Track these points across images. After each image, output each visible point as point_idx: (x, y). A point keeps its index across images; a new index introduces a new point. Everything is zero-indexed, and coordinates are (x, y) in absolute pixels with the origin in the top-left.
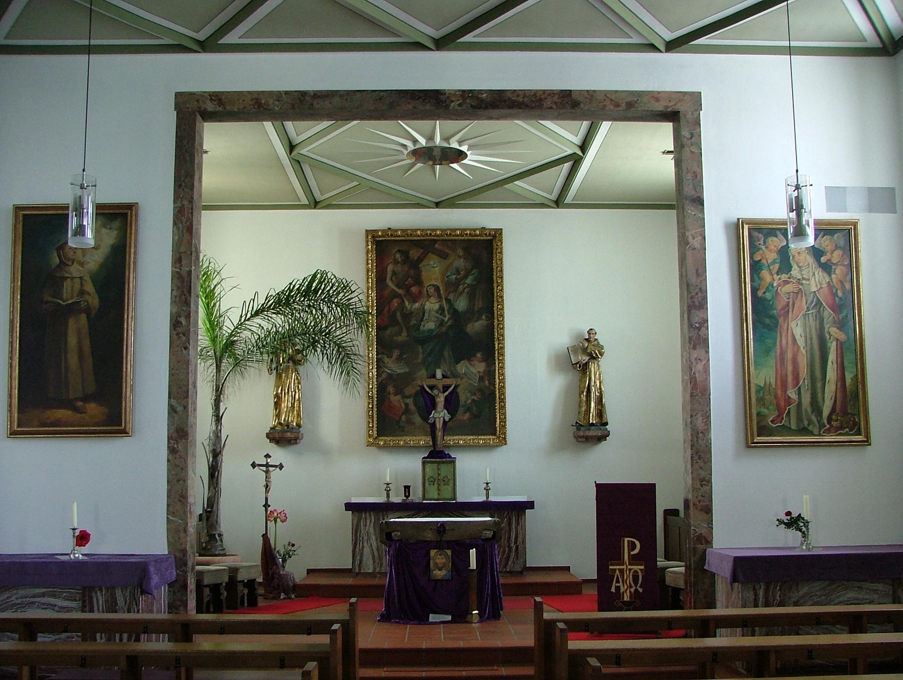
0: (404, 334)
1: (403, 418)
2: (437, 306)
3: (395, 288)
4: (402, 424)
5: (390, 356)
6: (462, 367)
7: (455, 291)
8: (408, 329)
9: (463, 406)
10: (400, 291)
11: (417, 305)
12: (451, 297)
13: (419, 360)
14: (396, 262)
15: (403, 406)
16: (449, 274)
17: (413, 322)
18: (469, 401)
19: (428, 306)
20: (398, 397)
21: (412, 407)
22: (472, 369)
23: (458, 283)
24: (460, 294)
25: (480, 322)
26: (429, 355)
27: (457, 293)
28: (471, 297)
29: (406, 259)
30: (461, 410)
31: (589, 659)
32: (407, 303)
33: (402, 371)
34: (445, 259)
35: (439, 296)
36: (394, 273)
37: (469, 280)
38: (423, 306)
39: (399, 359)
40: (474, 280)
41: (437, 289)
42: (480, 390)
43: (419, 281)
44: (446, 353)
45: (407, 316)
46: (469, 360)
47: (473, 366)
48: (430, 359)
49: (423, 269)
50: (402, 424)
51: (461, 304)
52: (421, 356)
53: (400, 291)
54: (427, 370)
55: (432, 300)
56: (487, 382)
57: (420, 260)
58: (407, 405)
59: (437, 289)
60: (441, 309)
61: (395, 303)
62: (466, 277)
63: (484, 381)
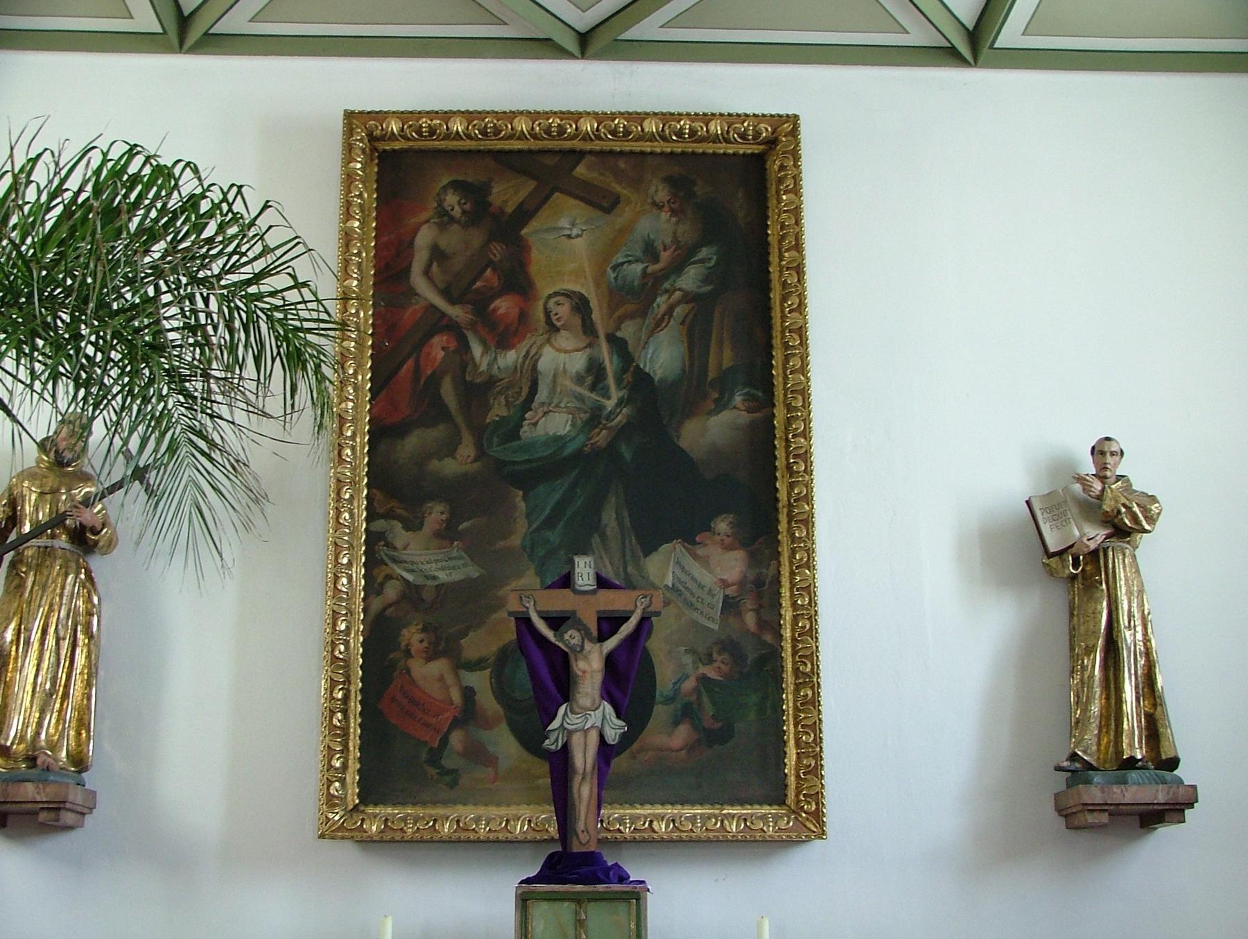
0: (467, 450)
1: (456, 739)
2: (578, 362)
4: (448, 762)
5: (413, 525)
7: (643, 313)
8: (480, 433)
9: (669, 700)
10: (456, 312)
11: (510, 358)
12: (628, 331)
13: (516, 540)
14: (444, 219)
15: (456, 696)
17: (498, 410)
18: (689, 684)
19: (549, 359)
20: (439, 666)
21: (488, 701)
22: (696, 570)
24: (658, 325)
25: (726, 416)
26: (550, 523)
27: (649, 321)
31: (435, 464)
32: (477, 350)
33: (457, 576)
34: (608, 211)
35: (588, 328)
36: (437, 254)
37: (690, 279)
39: (447, 534)
40: (706, 280)
41: (581, 305)
42: (730, 646)
43: (517, 280)
44: (609, 517)
45: (477, 392)
46: (689, 538)
47: (704, 561)
48: (554, 536)
50: (448, 762)
52: (521, 527)
53: (456, 312)
55: (565, 340)
56: (750, 620)
57: (524, 214)
59: (581, 305)
60: (595, 371)
61: (438, 348)
62: (678, 267)
63: (739, 614)
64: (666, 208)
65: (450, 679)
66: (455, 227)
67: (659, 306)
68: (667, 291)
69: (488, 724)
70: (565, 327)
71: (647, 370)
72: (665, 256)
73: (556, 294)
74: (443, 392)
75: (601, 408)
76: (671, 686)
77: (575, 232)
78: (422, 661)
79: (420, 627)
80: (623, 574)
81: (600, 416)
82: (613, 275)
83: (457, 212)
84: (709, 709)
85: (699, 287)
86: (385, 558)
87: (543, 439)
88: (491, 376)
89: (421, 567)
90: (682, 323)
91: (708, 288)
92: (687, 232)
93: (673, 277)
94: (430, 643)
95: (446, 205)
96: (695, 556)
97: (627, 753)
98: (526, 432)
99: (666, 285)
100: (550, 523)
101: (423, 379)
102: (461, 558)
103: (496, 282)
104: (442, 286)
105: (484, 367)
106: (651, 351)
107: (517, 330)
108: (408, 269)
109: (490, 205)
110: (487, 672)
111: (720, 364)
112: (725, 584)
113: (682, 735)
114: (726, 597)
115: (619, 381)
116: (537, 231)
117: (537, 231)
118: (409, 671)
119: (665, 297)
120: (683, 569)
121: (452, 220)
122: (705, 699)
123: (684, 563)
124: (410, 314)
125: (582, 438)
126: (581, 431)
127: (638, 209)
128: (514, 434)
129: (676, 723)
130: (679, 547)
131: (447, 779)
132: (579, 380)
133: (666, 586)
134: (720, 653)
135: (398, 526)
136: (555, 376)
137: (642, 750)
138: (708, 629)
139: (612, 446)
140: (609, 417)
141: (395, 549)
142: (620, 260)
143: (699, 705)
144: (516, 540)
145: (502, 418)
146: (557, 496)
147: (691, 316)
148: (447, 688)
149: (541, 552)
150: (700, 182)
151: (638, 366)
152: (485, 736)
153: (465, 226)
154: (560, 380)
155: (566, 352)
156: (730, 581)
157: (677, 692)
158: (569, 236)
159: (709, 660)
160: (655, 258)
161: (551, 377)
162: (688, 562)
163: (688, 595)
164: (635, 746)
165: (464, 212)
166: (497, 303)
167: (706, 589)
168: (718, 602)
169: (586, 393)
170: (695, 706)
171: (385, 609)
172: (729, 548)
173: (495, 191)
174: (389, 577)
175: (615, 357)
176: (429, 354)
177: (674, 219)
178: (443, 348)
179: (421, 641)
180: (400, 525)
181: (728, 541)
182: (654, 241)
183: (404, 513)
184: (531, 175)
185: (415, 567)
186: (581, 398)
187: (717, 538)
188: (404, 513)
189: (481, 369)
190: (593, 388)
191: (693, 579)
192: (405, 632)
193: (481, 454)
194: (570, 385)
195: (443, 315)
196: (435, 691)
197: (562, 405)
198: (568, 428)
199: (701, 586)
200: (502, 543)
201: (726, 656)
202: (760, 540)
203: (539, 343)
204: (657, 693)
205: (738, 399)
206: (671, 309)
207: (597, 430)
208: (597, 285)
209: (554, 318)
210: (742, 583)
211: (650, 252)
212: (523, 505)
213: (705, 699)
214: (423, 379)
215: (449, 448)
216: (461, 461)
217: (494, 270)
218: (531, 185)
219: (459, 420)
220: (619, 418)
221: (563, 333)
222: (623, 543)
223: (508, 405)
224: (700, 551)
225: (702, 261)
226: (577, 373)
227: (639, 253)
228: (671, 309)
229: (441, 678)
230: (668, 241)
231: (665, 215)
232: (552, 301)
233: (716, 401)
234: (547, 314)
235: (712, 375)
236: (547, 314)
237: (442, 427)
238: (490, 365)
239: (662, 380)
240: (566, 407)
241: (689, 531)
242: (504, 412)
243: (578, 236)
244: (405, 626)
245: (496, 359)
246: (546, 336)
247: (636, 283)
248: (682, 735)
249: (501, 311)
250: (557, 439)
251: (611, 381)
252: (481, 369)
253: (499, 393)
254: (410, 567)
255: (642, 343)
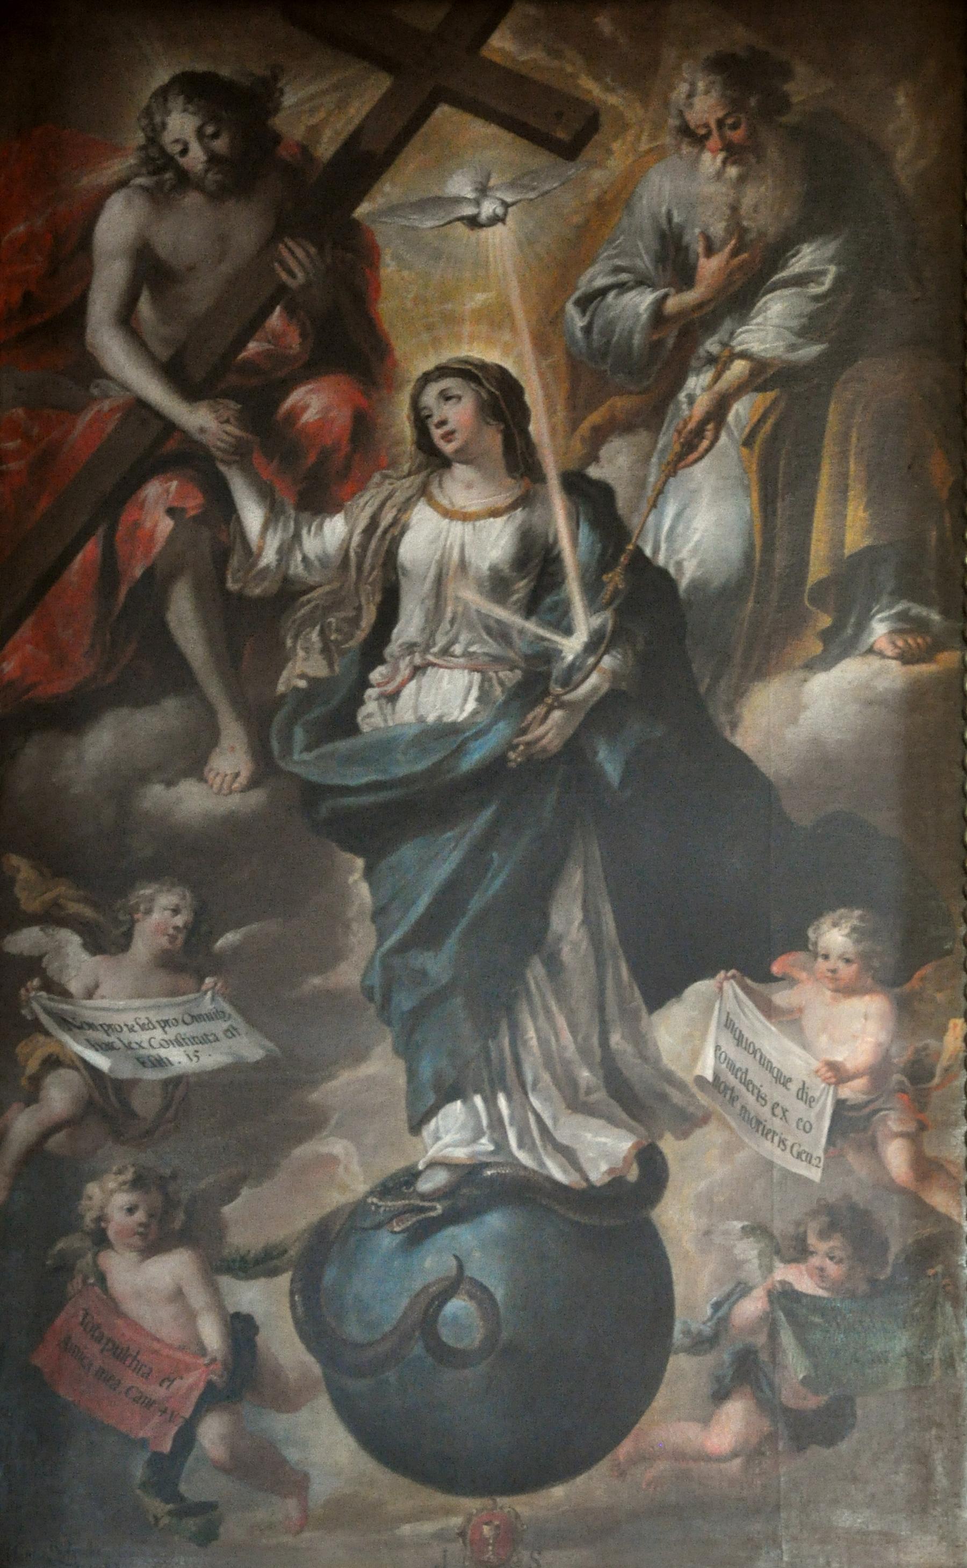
0: (231, 760)
1: (212, 1432)
2: (494, 543)
3: (155, 391)
4: (195, 1486)
5: (107, 939)
6: (693, 1034)
7: (654, 414)
8: (260, 722)
9: (701, 1344)
10: (200, 420)
11: (334, 532)
12: (615, 465)
13: (349, 974)
14: (164, 175)
15: (211, 1334)
16: (596, 277)
17: (304, 665)
18: (751, 1307)
19: (424, 537)
20: (174, 1268)
21: (284, 1345)
22: (772, 1041)
23: (676, 345)
24: (690, 447)
25: (850, 671)
26: (428, 933)
27: (667, 438)
28: (781, 479)
29: (252, 156)
30: (684, 1372)
31: (155, 795)
32: (252, 516)
33: (212, 1059)
34: (570, 151)
35: (520, 460)
36: (151, 271)
37: (768, 329)
38: (382, 544)
39: (187, 960)
40: (808, 330)
41: (502, 399)
42: (849, 1223)
43: (349, 340)
44: (567, 919)
45: (255, 618)
46: (757, 971)
47: (790, 1021)
48: (437, 964)
49: (389, 239)
50: (195, 1486)
51: (699, 526)
52: (362, 941)
53: (200, 420)
54: (407, 1050)
55: (464, 488)
56: (897, 1157)
57: (363, 164)
58: (241, 1329)
59: (502, 399)
60: (534, 574)
61: (158, 510)
62: (739, 298)
63: (872, 1148)
64: (714, 141)
65: (198, 1297)
66: (193, 199)
67: (691, 399)
68: (712, 360)
69: (286, 1399)
70: (465, 456)
71: (661, 560)
72: (710, 268)
73: (442, 371)
74: (172, 618)
75: (549, 655)
76: (709, 1311)
77: (488, 208)
78: (133, 1256)
79: (129, 1175)
80: (598, 1052)
81: (547, 676)
82: (579, 322)
83: (196, 158)
84: (795, 1365)
85: (792, 348)
86: (45, 1019)
87: (412, 732)
88: (286, 580)
89: (127, 1036)
90: (748, 442)
91: (812, 351)
92: (764, 202)
93: (727, 324)
94: (151, 1216)
95: (168, 138)
96: (769, 1010)
97: (602, 1468)
98: (371, 714)
99: (711, 345)
100: (428, 933)
101: (123, 591)
102: (218, 1015)
103: (294, 342)
104: (164, 353)
105: (269, 557)
106: (670, 510)
107: (348, 468)
108: (80, 308)
109: (277, 139)
110: (284, 1281)
111: (838, 543)
112: (837, 1074)
113: (731, 1426)
114: (840, 1105)
115: (592, 588)
116: (392, 210)
117: (392, 210)
118: (102, 1279)
119: (706, 377)
120: (740, 1040)
121: (184, 179)
122: (787, 1338)
123: (742, 1024)
124: (89, 427)
125: (502, 730)
126: (502, 712)
127: (644, 146)
128: (343, 722)
129: (720, 1396)
130: (731, 988)
131: (191, 1524)
132: (498, 586)
133: (700, 1080)
134: (824, 1235)
135: (72, 941)
136: (439, 580)
137: (642, 1458)
138: (798, 1179)
139: (574, 751)
140: (571, 677)
141: (66, 994)
142: (600, 282)
143: (773, 1355)
144: (349, 974)
145: (314, 682)
146: (441, 872)
147: (770, 421)
148: (191, 1316)
149: (405, 1001)
150: (800, 69)
151: (639, 551)
152: (279, 1424)
153: (217, 196)
154: (451, 589)
155: (465, 517)
156: (850, 1066)
157: (722, 1323)
158: (473, 222)
159: (799, 1251)
160: (684, 276)
161: (428, 585)
162: (752, 1020)
163: (751, 1099)
164: (625, 1448)
165: (213, 159)
166: (296, 397)
167: (794, 1087)
168: (820, 1115)
169: (517, 621)
170: (764, 1357)
171: (46, 1135)
172: (848, 990)
173: (289, 100)
174: (53, 1063)
175: (584, 530)
176: (137, 525)
177: (733, 171)
178: (171, 512)
179: (131, 1210)
180: (76, 939)
181: (847, 972)
182: (682, 228)
183: (88, 912)
184: (386, 64)
185: (112, 1039)
186: (501, 633)
187: (821, 965)
188: (88, 912)
189: (263, 562)
190: (530, 608)
191: (765, 1063)
192: (93, 1189)
193: (265, 767)
194: (471, 597)
195: (170, 427)
196: (158, 1320)
197: (458, 649)
198: (471, 706)
199: (783, 1080)
200: (316, 981)
201: (836, 1242)
202: (927, 970)
203: (399, 497)
204: (678, 1327)
205: (879, 630)
206: (718, 413)
207: (540, 710)
208: (542, 345)
209: (437, 433)
210: (878, 1073)
211: (674, 257)
212: (364, 890)
213: (787, 1338)
214: (123, 591)
215: (193, 759)
216: (218, 789)
217: (291, 311)
218: (378, 85)
219: (213, 688)
220: (594, 679)
221: (460, 471)
222: (601, 980)
223: (326, 650)
224: (782, 997)
225: (800, 280)
226: (494, 569)
227: (645, 262)
228: (718, 413)
229: (178, 1295)
230: (718, 229)
231: (710, 161)
232: (430, 396)
233: (827, 636)
234: (421, 421)
235: (817, 571)
236: (421, 421)
237: (171, 704)
238: (284, 552)
239: (697, 586)
240: (466, 654)
241: (753, 948)
242: (317, 667)
243: (495, 220)
244: (94, 1176)
245: (297, 537)
246: (418, 479)
247: (637, 340)
248: (731, 1426)
249: (309, 416)
250: (446, 731)
251: (573, 589)
252: (263, 562)
253: (308, 621)
254: (101, 1036)
255: (650, 493)
